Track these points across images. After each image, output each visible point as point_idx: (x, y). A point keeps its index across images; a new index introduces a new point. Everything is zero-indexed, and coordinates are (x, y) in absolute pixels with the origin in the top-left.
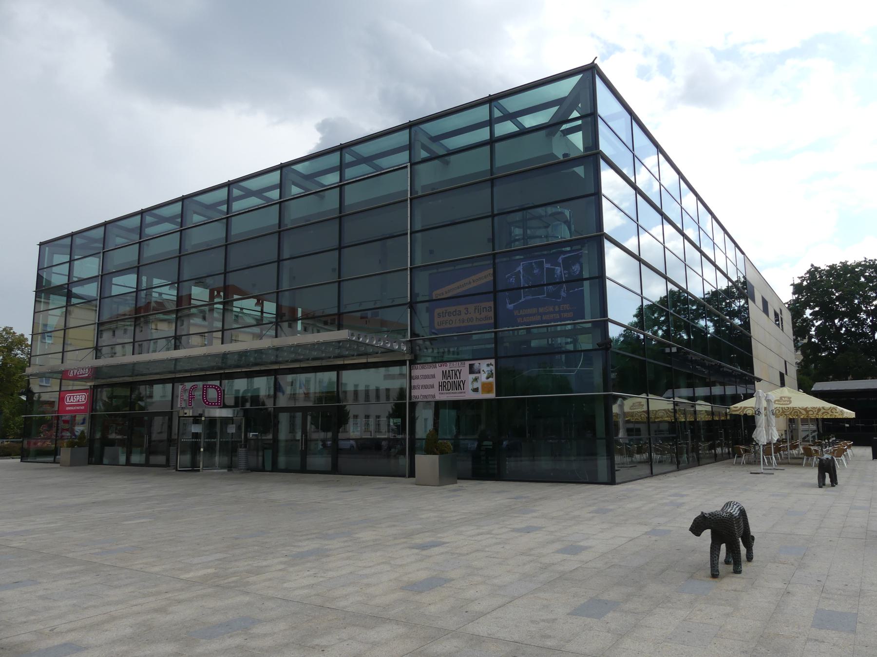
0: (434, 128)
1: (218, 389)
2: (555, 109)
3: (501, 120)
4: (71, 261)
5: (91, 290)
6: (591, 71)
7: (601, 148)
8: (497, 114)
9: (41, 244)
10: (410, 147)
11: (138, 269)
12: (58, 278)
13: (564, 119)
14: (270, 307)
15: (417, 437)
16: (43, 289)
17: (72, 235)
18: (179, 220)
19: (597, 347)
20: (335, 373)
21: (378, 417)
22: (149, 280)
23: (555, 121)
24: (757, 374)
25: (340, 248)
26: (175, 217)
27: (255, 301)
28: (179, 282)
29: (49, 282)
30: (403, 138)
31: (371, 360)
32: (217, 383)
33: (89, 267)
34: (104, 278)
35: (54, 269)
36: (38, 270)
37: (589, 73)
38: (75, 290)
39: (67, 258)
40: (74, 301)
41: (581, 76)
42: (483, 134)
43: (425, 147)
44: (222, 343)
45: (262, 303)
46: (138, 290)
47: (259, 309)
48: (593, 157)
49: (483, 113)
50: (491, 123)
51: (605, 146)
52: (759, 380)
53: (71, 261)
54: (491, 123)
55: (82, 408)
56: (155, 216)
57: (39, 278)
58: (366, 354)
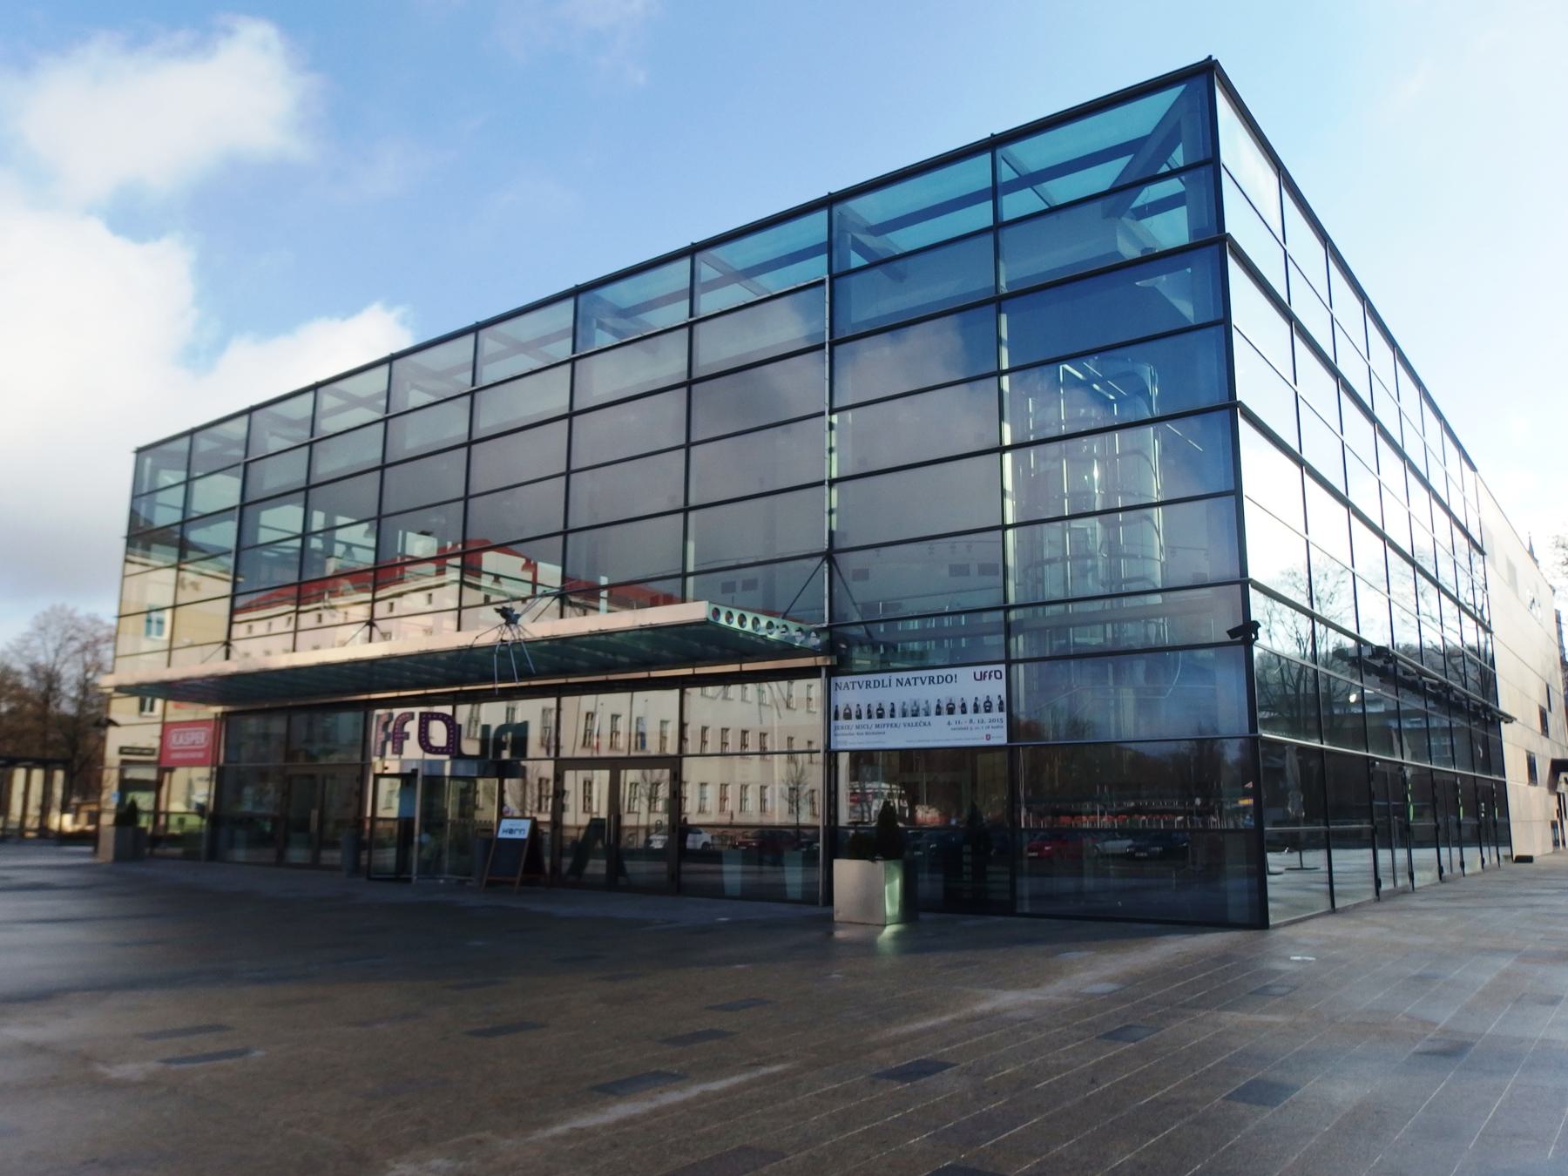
0: (871, 208)
1: (450, 721)
2: (1123, 162)
3: (1014, 186)
4: (188, 482)
5: (223, 534)
6: (1204, 78)
7: (1231, 227)
8: (1006, 174)
9: (139, 451)
10: (829, 247)
11: (306, 492)
12: (166, 515)
13: (1149, 174)
14: (550, 574)
15: (1335, 853)
16: (141, 536)
17: (192, 433)
18: (383, 402)
19: (1227, 638)
20: (676, 692)
21: (703, 785)
22: (329, 517)
23: (1127, 181)
24: (1505, 705)
25: (688, 445)
26: (376, 397)
27: (523, 561)
28: (379, 521)
29: (149, 522)
30: (815, 228)
31: (747, 667)
32: (447, 710)
33: (221, 491)
34: (245, 510)
35: (160, 497)
36: (135, 497)
37: (1200, 82)
38: (196, 535)
39: (182, 476)
40: (191, 555)
41: (1181, 88)
42: (981, 215)
43: (860, 248)
44: (459, 629)
45: (535, 566)
46: (306, 535)
47: (528, 576)
48: (1213, 246)
49: (976, 173)
50: (995, 192)
51: (1238, 223)
52: (1509, 719)
53: (188, 482)
54: (995, 192)
55: (201, 755)
56: (340, 394)
57: (133, 514)
58: (741, 657)
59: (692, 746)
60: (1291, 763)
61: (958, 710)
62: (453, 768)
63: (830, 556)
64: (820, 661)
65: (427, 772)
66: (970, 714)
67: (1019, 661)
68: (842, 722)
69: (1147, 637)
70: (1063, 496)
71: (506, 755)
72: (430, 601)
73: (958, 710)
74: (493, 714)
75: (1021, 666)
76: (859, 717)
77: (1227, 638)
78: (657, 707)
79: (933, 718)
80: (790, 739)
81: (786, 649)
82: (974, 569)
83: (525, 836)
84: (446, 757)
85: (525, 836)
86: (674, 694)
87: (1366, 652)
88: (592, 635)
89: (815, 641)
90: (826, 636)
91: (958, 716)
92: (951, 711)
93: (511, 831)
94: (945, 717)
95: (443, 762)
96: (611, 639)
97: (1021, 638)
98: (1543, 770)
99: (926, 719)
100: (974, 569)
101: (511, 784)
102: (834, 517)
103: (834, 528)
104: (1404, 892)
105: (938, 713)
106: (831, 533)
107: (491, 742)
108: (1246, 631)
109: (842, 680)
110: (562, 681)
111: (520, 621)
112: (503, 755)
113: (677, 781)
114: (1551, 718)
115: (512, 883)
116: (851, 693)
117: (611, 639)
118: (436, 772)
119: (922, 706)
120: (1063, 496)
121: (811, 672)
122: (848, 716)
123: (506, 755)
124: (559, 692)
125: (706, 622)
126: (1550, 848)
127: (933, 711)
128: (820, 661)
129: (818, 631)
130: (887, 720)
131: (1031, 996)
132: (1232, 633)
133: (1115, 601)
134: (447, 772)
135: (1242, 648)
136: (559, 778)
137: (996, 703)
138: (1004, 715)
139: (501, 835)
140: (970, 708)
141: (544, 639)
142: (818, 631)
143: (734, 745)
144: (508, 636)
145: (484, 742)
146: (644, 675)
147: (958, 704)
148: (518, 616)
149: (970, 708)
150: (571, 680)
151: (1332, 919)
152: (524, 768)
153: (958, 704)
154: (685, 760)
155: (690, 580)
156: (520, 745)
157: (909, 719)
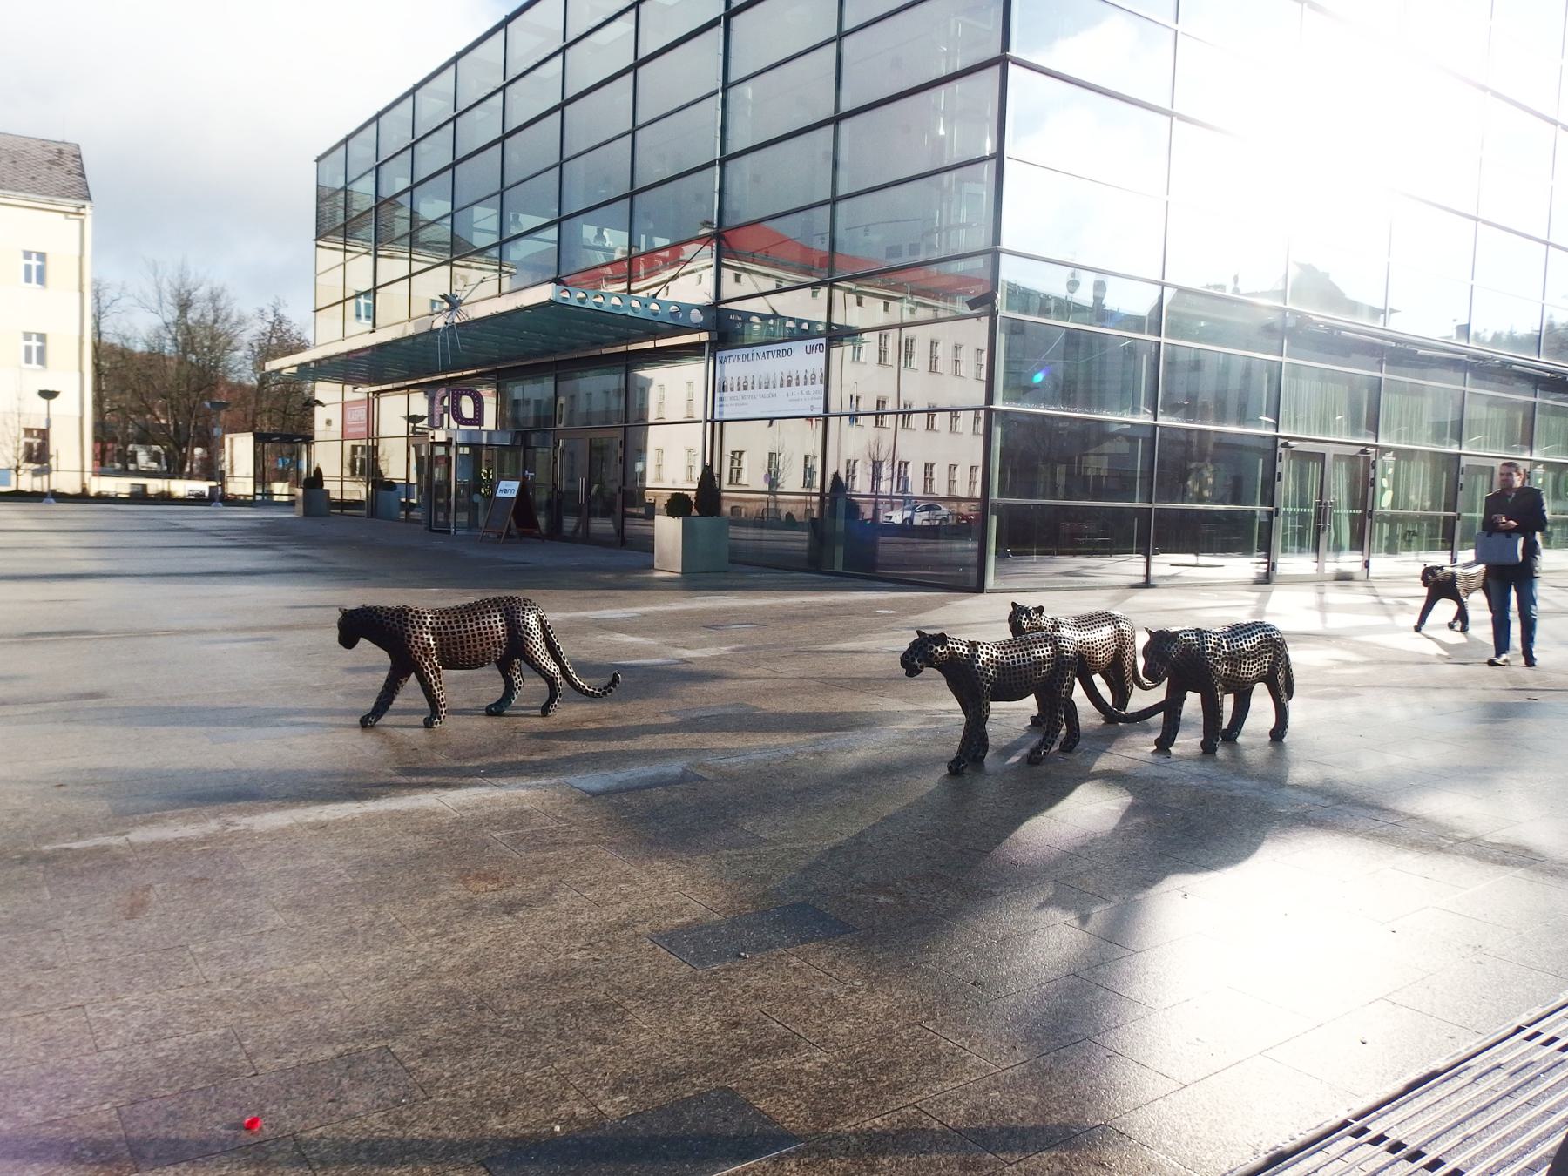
90: (713, 314)
91: (794, 388)
94: (786, 389)
116: (734, 367)
121: (694, 350)
130: (749, 392)
137: (818, 375)
149: (802, 380)
157: (764, 391)
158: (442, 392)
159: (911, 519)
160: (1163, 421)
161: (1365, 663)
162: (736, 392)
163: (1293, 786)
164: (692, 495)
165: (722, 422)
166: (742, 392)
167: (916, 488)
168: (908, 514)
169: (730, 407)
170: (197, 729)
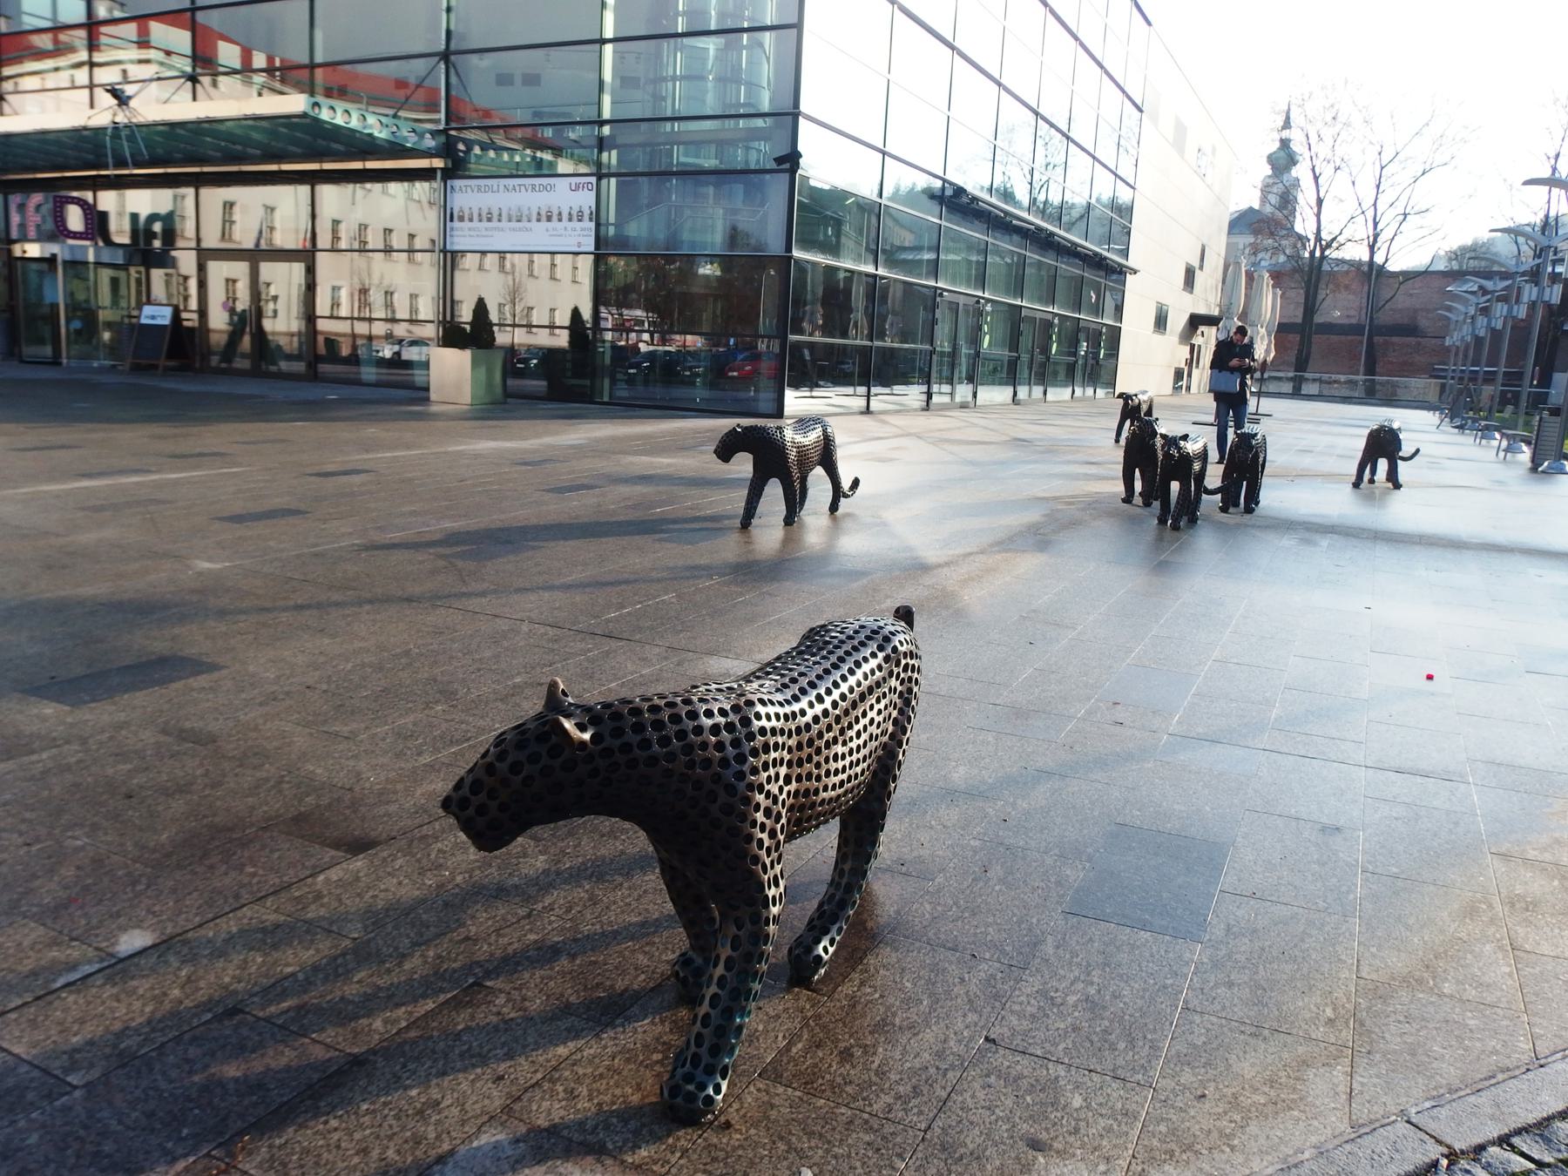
31: (371, 165)
32: (88, 196)
59: (324, 241)
60: (896, 294)
61: (555, 218)
62: (97, 254)
63: (445, 56)
64: (438, 163)
65: (68, 258)
66: (565, 222)
67: (610, 175)
68: (456, 224)
69: (747, 162)
70: (677, 14)
71: (157, 244)
72: (124, 71)
73: (555, 218)
74: (145, 202)
75: (613, 181)
76: (471, 220)
77: (774, 166)
78: (288, 201)
79: (534, 223)
80: (412, 236)
81: (396, 149)
82: (518, 80)
83: (167, 322)
84: (87, 243)
85: (167, 322)
86: (304, 190)
87: (949, 192)
88: (199, 122)
89: (429, 142)
90: (442, 139)
91: (555, 223)
92: (549, 219)
93: (153, 317)
94: (544, 224)
95: (86, 247)
96: (215, 126)
97: (614, 153)
98: (1177, 322)
99: (528, 225)
100: (518, 80)
101: (157, 275)
102: (453, 16)
103: (452, 27)
104: (964, 406)
105: (539, 220)
106: (448, 32)
107: (141, 230)
108: (790, 160)
109: (458, 183)
110: (197, 170)
111: (132, 103)
112: (151, 246)
113: (311, 271)
114: (1199, 277)
115: (155, 367)
116: (466, 195)
117: (215, 126)
118: (79, 258)
119: (526, 212)
120: (677, 14)
121: (426, 175)
122: (461, 219)
123: (157, 244)
124: (198, 181)
125: (304, 115)
126: (1168, 388)
127: (534, 217)
128: (438, 163)
129: (434, 134)
130: (494, 224)
131: (492, 444)
132: (779, 160)
133: (732, 122)
134: (91, 258)
135: (787, 176)
136: (201, 268)
137: (587, 213)
138: (592, 225)
139: (144, 321)
140: (565, 216)
141: (156, 124)
142: (434, 134)
143: (375, 240)
144: (121, 118)
145: (135, 232)
146: (274, 167)
147: (555, 212)
148: (129, 98)
149: (565, 216)
150: (206, 169)
151: (865, 419)
152: (174, 258)
153: (555, 212)
154: (318, 254)
155: (319, 72)
156: (170, 236)
157: (514, 224)
158: (37, 198)
159: (398, 354)
160: (881, 272)
161: (468, 595)
162: (475, 224)
163: (839, 574)
164: (468, 327)
165: (453, 252)
166: (485, 224)
167: (402, 313)
168: (396, 348)
169: (462, 238)
170: (622, 518)
